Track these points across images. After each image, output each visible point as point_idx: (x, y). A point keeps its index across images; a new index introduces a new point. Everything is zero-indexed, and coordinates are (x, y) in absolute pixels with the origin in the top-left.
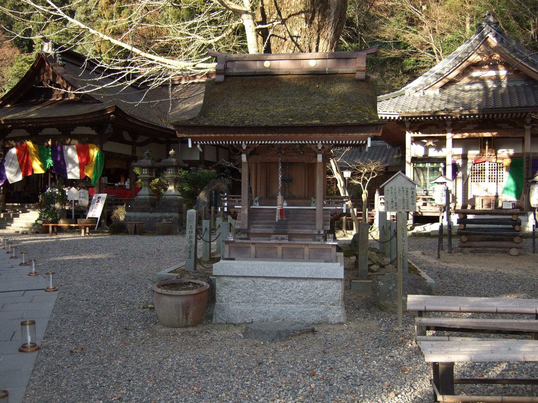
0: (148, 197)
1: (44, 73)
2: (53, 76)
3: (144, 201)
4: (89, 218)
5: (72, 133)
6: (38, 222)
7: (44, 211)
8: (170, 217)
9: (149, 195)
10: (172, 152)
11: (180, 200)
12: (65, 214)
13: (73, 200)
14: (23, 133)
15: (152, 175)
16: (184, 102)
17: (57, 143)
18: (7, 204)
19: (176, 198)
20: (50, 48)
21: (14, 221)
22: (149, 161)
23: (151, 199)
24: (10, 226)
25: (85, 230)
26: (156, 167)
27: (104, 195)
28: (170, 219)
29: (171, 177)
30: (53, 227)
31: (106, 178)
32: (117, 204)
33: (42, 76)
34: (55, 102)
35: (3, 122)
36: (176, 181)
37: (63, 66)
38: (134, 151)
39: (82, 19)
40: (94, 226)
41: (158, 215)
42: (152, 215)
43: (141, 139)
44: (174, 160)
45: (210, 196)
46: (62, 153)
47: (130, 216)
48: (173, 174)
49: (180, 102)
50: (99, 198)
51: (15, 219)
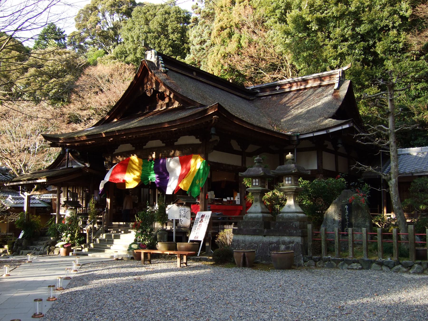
0: (260, 215)
1: (147, 82)
2: (156, 85)
3: (254, 221)
4: (192, 241)
5: (176, 143)
6: (133, 246)
7: (139, 234)
8: (290, 242)
9: (262, 212)
10: (289, 155)
11: (303, 218)
12: (166, 236)
13: (174, 219)
14: (128, 147)
15: (264, 187)
16: (297, 107)
17: (160, 155)
18: (113, 223)
19: (297, 216)
20: (153, 56)
21: (114, 243)
22: (261, 169)
23: (264, 217)
24: (109, 248)
25: (182, 259)
26: (270, 177)
27: (209, 214)
28: (290, 245)
29: (290, 189)
30: (145, 254)
31: (213, 192)
32: (225, 224)
33: (145, 86)
34: (159, 111)
35: (104, 136)
36: (296, 193)
37: (166, 72)
38: (244, 161)
39: (198, 49)
40: (195, 252)
41: (274, 239)
42: (267, 239)
43: (251, 148)
44: (293, 165)
45: (342, 212)
46: (164, 166)
47: (238, 241)
48: (291, 185)
49: (292, 108)
50: (203, 216)
51: (116, 241)
